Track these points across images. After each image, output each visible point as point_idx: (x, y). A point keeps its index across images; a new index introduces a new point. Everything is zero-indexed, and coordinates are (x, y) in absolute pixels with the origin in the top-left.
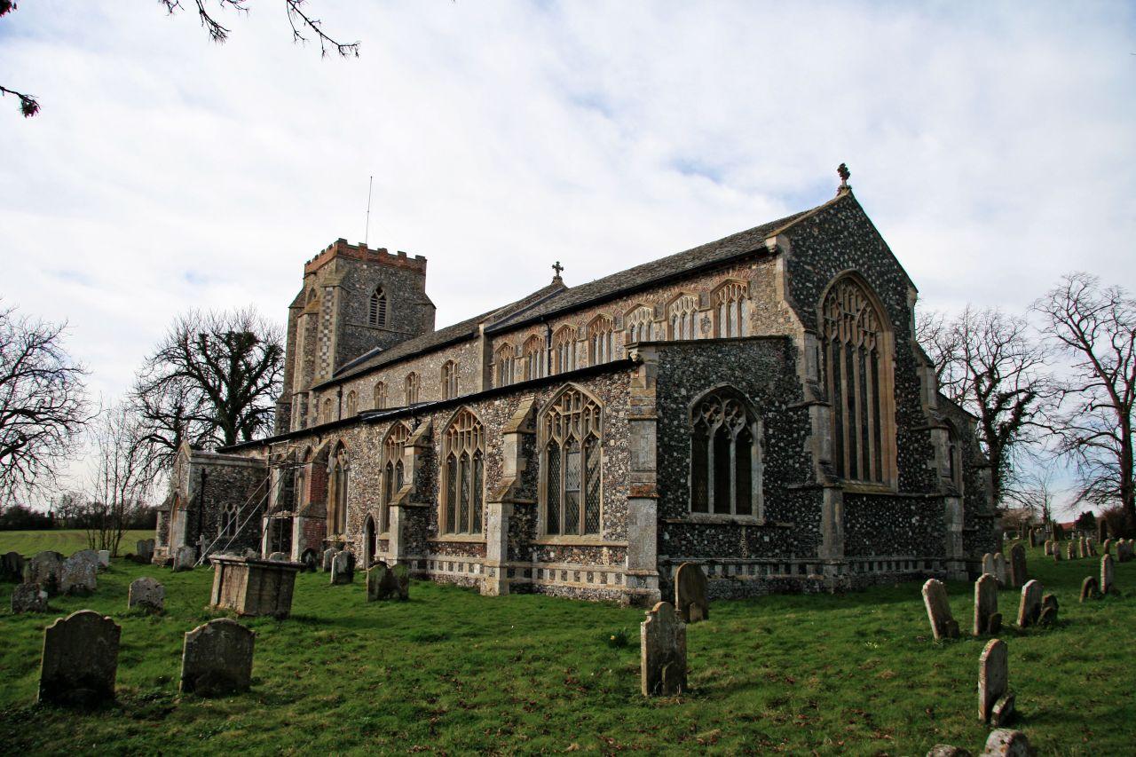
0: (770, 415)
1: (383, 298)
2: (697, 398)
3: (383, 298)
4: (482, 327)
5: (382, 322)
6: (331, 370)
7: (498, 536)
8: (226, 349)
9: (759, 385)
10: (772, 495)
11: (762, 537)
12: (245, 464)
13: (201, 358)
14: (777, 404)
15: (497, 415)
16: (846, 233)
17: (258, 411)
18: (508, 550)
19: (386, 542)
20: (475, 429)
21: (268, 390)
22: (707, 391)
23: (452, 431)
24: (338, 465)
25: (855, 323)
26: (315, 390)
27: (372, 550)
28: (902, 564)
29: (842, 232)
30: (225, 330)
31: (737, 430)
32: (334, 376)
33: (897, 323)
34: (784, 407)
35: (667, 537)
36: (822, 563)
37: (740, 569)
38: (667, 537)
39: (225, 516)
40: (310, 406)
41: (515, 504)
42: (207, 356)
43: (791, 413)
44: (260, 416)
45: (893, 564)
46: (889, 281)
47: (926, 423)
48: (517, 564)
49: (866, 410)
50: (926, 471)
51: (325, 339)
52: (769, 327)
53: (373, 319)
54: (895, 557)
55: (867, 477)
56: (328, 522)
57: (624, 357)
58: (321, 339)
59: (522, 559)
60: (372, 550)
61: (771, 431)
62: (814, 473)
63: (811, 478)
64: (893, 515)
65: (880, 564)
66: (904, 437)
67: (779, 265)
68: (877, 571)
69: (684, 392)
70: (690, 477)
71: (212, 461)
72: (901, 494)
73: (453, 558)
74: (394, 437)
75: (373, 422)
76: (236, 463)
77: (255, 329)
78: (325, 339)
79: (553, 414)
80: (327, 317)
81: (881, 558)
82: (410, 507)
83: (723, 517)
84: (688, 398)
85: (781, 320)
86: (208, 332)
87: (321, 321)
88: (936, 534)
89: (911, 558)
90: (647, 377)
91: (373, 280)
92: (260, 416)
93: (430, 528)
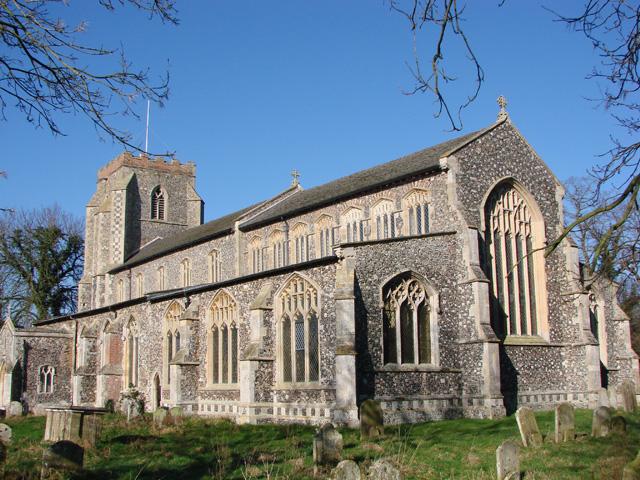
0: (443, 290)
1: (161, 197)
2: (386, 281)
3: (161, 197)
4: (237, 224)
5: (161, 217)
6: (122, 256)
7: (248, 383)
8: (37, 242)
9: (435, 268)
10: (446, 349)
11: (439, 379)
12: (57, 335)
13: (17, 251)
14: (449, 282)
15: (246, 295)
16: (503, 150)
17: (63, 290)
18: (256, 395)
19: (167, 393)
20: (230, 306)
21: (72, 272)
22: (394, 275)
23: (214, 307)
24: (130, 334)
25: (512, 216)
26: (111, 273)
27: (159, 400)
28: (554, 397)
29: (500, 149)
30: (35, 225)
31: (418, 302)
32: (125, 261)
33: (547, 214)
34: (454, 284)
35: (365, 381)
36: (484, 397)
37: (422, 403)
38: (365, 381)
39: (42, 376)
40: (107, 287)
41: (260, 361)
42: (21, 248)
43: (460, 288)
44: (66, 294)
45: (547, 397)
46: (540, 183)
47: (571, 290)
48: (261, 404)
49: (217, 344)
50: (572, 326)
51: (117, 232)
52: (443, 224)
53: (153, 216)
54: (549, 391)
55: (524, 331)
56: (123, 378)
57: (331, 254)
58: (113, 232)
59: (266, 400)
60: (159, 400)
61: (444, 302)
62: (476, 332)
63: (475, 335)
64: (547, 360)
65: (536, 396)
66: (554, 300)
67: (450, 178)
68: (555, 401)
69: (375, 277)
70: (382, 338)
71: (32, 334)
72: (552, 344)
73: (218, 402)
74: (172, 312)
75: (154, 301)
76: (51, 334)
77: (60, 223)
78: (117, 232)
79: (285, 294)
80: (118, 215)
81: (537, 392)
82: (185, 365)
83: (408, 366)
84: (379, 281)
85: (452, 219)
86: (21, 228)
87: (113, 218)
88: (580, 373)
89: (562, 391)
90: (348, 267)
91: (153, 183)
92: (66, 294)
93: (200, 380)
